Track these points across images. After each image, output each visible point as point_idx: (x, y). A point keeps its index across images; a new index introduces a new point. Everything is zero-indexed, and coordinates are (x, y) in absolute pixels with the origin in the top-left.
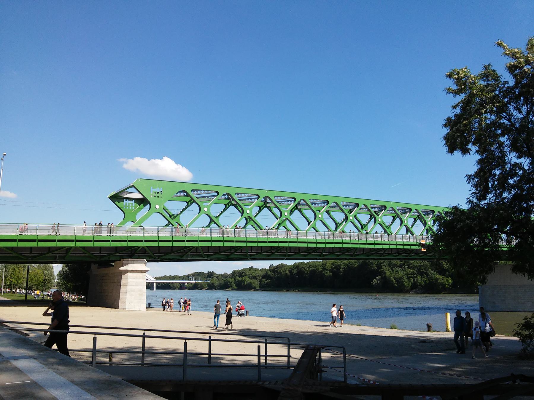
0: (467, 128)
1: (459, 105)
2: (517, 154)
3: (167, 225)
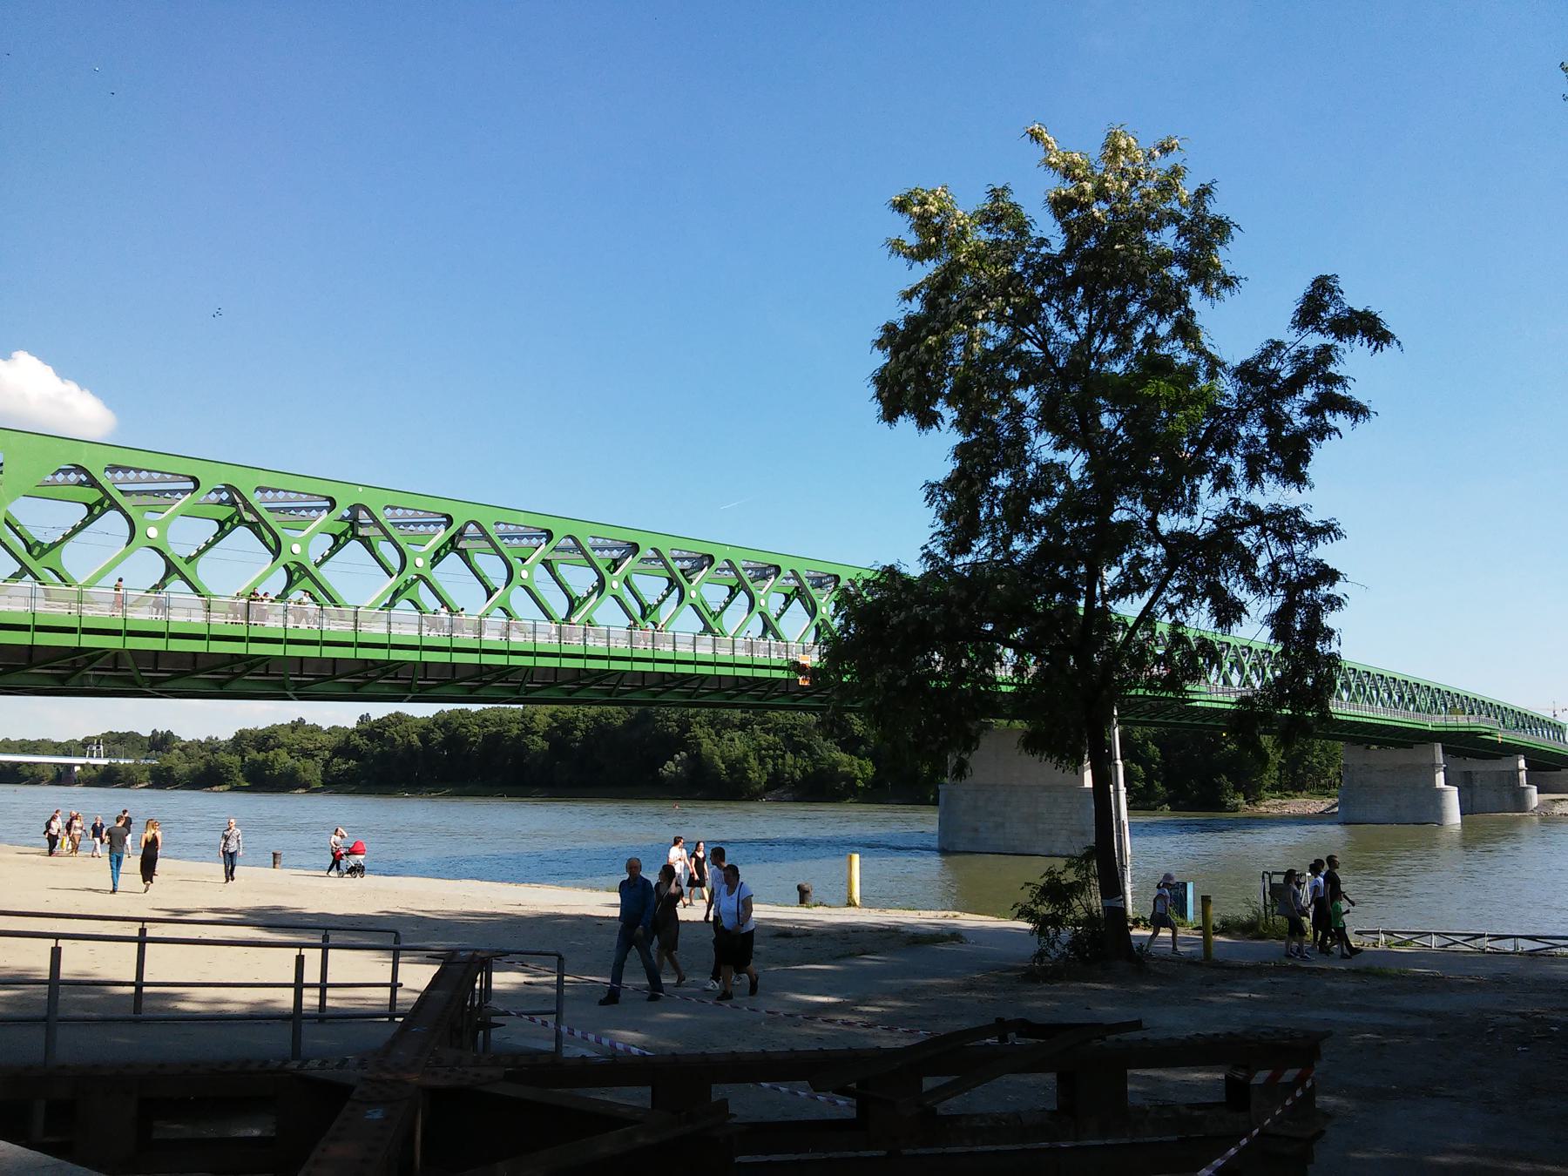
0: (935, 358)
1: (920, 292)
2: (1054, 437)
3: (16, 576)
